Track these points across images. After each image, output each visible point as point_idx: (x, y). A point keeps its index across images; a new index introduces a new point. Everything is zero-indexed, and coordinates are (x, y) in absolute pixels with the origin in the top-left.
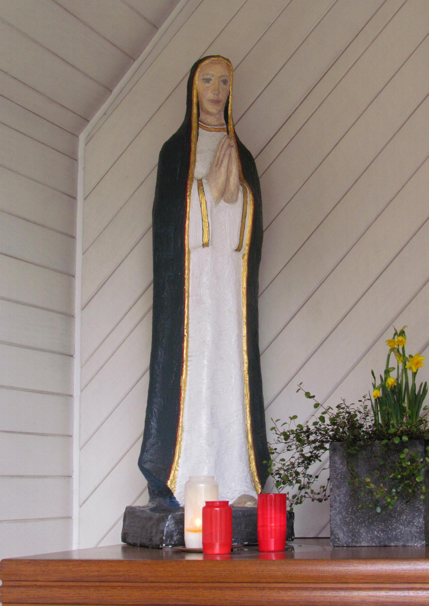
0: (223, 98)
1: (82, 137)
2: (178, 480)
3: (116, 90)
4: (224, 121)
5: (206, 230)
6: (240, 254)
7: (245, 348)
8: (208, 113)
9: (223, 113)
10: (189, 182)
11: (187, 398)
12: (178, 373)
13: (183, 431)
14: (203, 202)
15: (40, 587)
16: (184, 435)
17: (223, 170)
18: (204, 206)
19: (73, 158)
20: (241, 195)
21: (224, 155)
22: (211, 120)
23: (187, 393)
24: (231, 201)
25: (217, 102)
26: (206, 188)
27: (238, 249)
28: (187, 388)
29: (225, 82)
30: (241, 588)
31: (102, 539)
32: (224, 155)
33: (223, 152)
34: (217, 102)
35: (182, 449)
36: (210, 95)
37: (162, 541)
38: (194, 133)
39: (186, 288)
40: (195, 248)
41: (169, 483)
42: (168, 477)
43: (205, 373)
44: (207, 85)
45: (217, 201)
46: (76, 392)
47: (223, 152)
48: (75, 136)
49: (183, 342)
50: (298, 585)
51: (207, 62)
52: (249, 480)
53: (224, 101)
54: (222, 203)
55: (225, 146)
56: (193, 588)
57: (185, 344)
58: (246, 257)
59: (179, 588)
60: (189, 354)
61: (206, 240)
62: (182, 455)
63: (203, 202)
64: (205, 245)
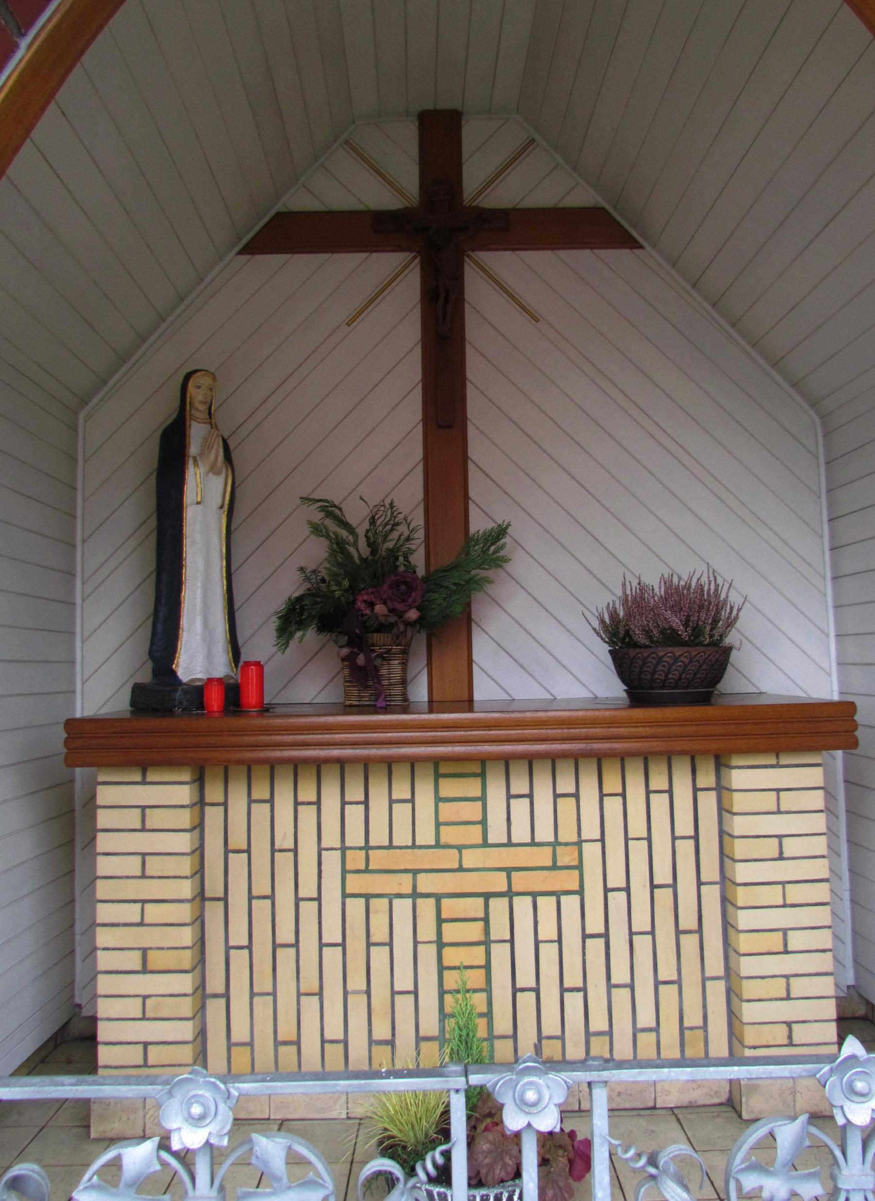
0: (209, 400)
1: (82, 416)
2: (180, 664)
3: (111, 383)
4: (208, 417)
5: (199, 492)
6: (222, 511)
7: (225, 575)
8: (198, 410)
9: (207, 412)
10: (187, 458)
11: (186, 608)
12: (179, 590)
13: (183, 631)
14: (198, 473)
15: (100, 737)
16: (185, 634)
17: (213, 452)
18: (198, 476)
19: (75, 429)
20: (224, 470)
21: (214, 442)
22: (197, 414)
23: (186, 605)
24: (218, 473)
25: (204, 403)
26: (200, 463)
27: (222, 507)
28: (186, 601)
29: (211, 389)
30: (255, 735)
31: (101, 707)
32: (214, 442)
33: (213, 440)
34: (204, 403)
35: (183, 642)
36: (200, 398)
37: (174, 706)
38: (188, 423)
39: (184, 532)
40: (191, 504)
41: (174, 666)
42: (172, 662)
43: (199, 592)
44: (198, 390)
45: (207, 473)
46: (78, 601)
47: (213, 440)
48: (77, 414)
49: (182, 569)
50: (300, 732)
51: (199, 374)
52: (229, 664)
53: (209, 402)
54: (211, 475)
55: (215, 435)
56: (219, 735)
57: (184, 571)
58: (226, 513)
59: (208, 735)
60: (187, 578)
61: (199, 499)
62: (183, 647)
63: (198, 473)
64: (198, 503)
